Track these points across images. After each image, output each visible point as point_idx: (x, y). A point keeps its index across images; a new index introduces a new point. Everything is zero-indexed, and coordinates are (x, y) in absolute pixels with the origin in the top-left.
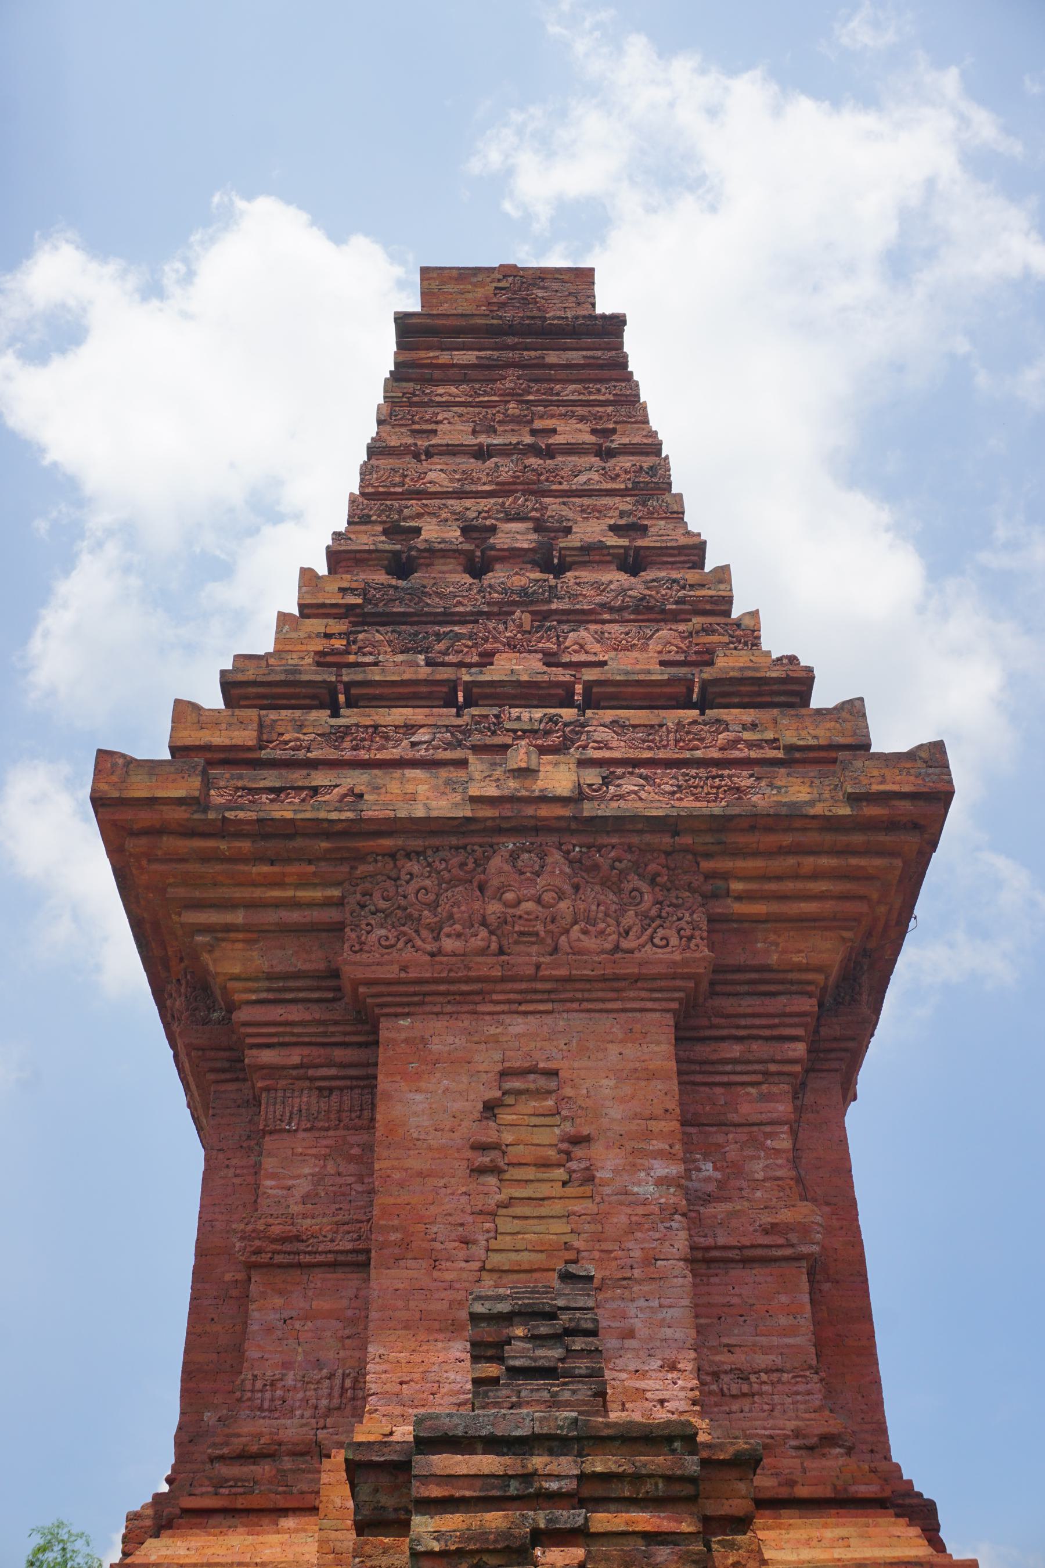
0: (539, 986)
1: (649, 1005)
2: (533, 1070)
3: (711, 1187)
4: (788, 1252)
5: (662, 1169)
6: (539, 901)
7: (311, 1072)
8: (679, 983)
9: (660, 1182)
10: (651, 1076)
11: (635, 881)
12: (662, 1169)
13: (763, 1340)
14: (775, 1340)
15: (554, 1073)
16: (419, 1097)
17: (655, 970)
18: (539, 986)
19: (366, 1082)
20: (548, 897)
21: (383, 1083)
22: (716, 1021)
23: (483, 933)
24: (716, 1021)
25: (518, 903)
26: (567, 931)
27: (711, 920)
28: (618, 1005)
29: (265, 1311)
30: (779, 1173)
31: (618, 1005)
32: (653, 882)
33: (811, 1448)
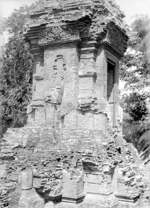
0: (60, 44)
1: (73, 45)
2: (60, 55)
3: (83, 67)
4: (90, 75)
5: (73, 67)
6: (58, 34)
7: (40, 56)
8: (76, 42)
9: (73, 69)
10: (73, 55)
11: (70, 29)
12: (73, 67)
13: (87, 86)
14: (88, 86)
15: (62, 56)
16: (48, 60)
17: (72, 41)
18: (60, 44)
19: (43, 57)
20: (59, 33)
21: (45, 58)
22: (84, 45)
23: (52, 38)
24: (84, 45)
25: (56, 34)
26: (62, 37)
27: (80, 32)
28: (70, 46)
29: (92, 59)
30: (91, 65)
31: (70, 46)
32: (72, 28)
33: (89, 98)
